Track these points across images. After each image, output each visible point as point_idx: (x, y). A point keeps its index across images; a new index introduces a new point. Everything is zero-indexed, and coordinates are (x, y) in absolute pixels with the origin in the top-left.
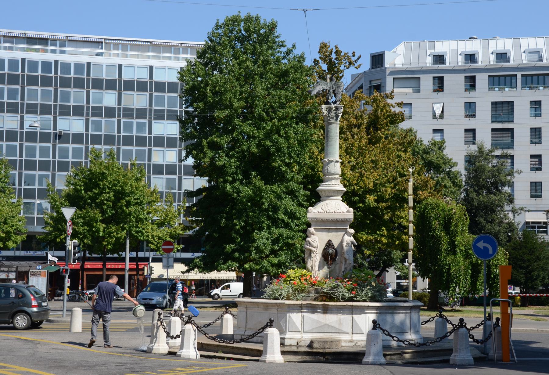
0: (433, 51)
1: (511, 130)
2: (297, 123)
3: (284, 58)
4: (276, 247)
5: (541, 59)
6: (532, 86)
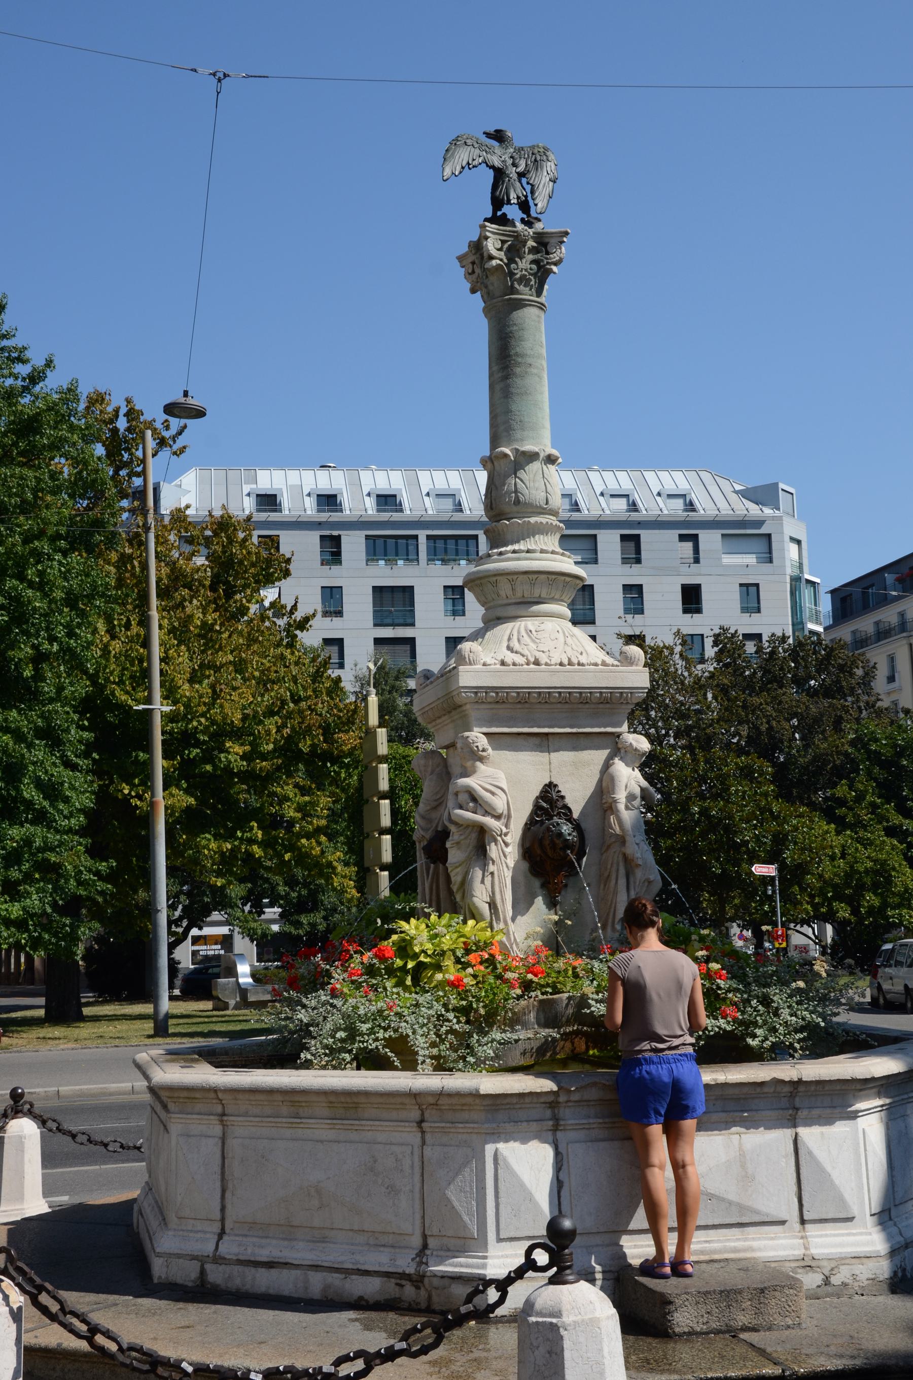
0: (254, 486)
1: (411, 642)
3: (25, 389)
4: (15, 874)
5: (459, 508)
6: (446, 558)
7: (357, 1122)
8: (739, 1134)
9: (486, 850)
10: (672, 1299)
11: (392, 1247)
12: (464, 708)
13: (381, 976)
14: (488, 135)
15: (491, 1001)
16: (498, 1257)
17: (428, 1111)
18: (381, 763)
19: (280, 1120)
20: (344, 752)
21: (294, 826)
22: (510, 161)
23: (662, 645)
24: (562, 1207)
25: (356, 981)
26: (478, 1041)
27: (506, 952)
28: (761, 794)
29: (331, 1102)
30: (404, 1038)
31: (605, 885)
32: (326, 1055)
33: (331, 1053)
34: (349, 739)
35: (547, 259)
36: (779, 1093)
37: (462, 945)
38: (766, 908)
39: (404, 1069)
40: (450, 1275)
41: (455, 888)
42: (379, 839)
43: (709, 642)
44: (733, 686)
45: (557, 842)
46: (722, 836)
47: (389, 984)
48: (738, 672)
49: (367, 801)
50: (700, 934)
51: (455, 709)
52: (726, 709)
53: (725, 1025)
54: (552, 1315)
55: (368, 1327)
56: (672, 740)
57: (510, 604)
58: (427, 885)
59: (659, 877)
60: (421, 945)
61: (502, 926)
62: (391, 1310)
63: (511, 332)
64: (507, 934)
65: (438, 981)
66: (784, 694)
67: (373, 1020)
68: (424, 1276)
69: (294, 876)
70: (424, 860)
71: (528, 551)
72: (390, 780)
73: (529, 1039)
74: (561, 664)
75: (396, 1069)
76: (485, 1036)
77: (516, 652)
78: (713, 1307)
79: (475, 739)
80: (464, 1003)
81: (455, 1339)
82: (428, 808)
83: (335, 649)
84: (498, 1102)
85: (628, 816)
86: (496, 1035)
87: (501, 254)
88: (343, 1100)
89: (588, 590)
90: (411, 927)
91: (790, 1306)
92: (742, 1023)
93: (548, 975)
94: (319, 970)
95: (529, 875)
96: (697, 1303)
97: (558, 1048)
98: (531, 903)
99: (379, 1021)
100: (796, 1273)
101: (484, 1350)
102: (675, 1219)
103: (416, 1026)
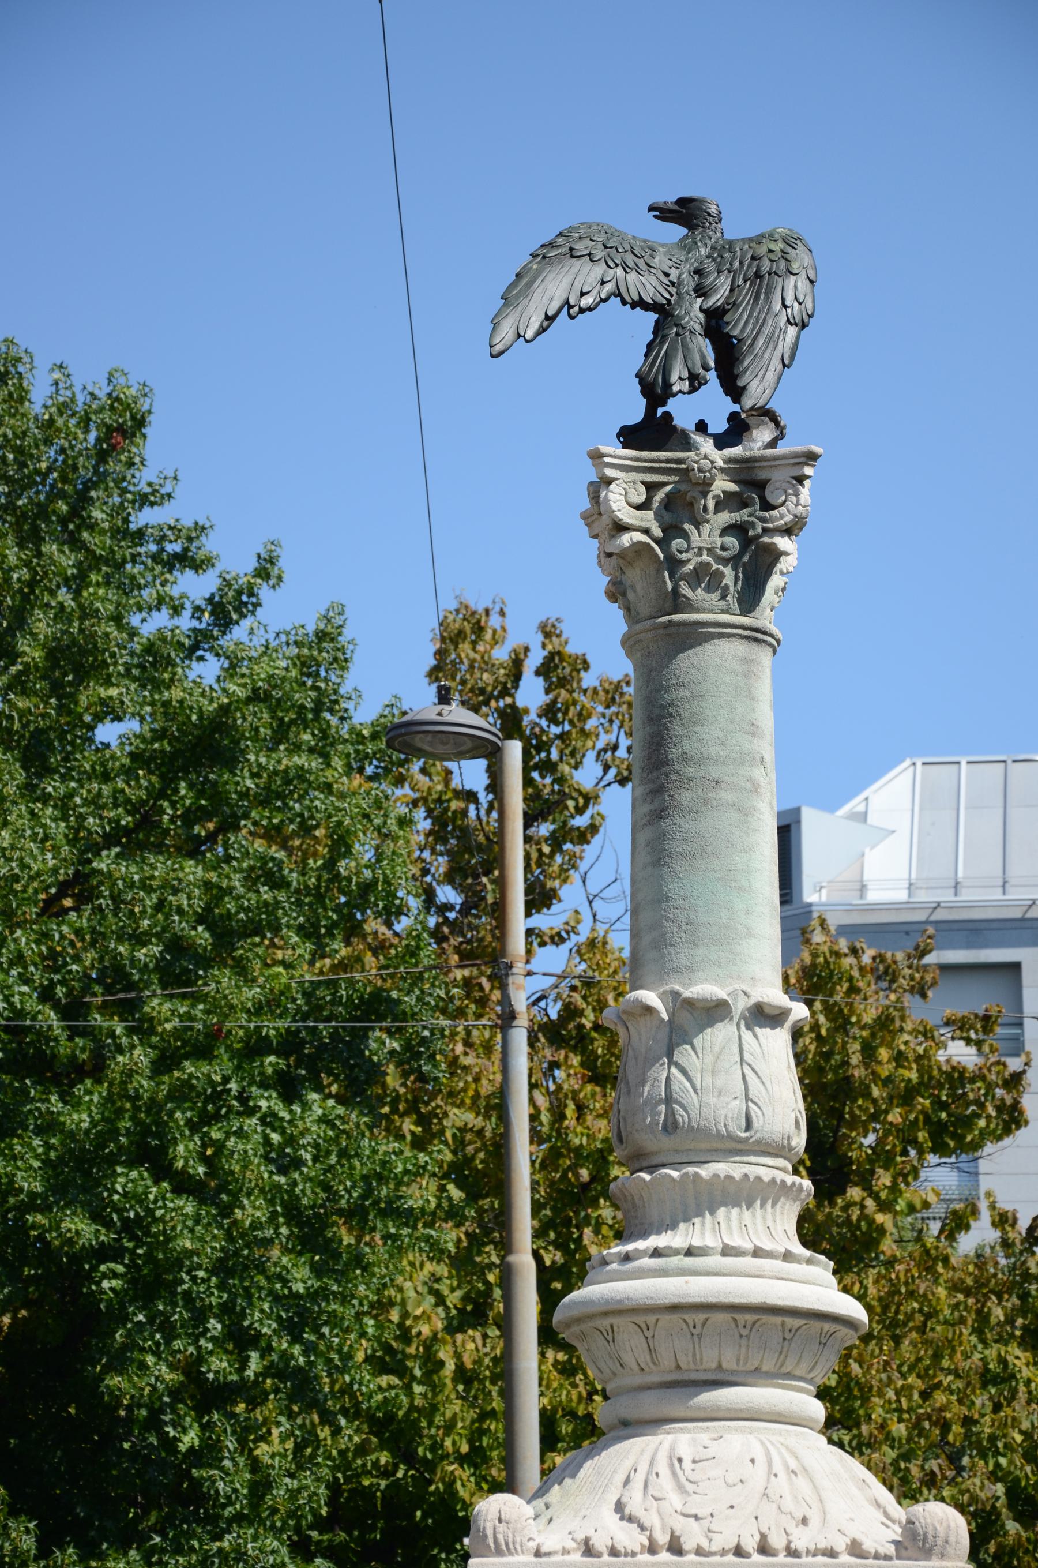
2: (289, 1089)
3: (198, 644)
14: (663, 213)
22: (689, 283)
35: (763, 520)
57: (649, 1387)
63: (672, 704)
71: (689, 1252)
74: (739, 1552)
77: (630, 1519)
87: (648, 519)
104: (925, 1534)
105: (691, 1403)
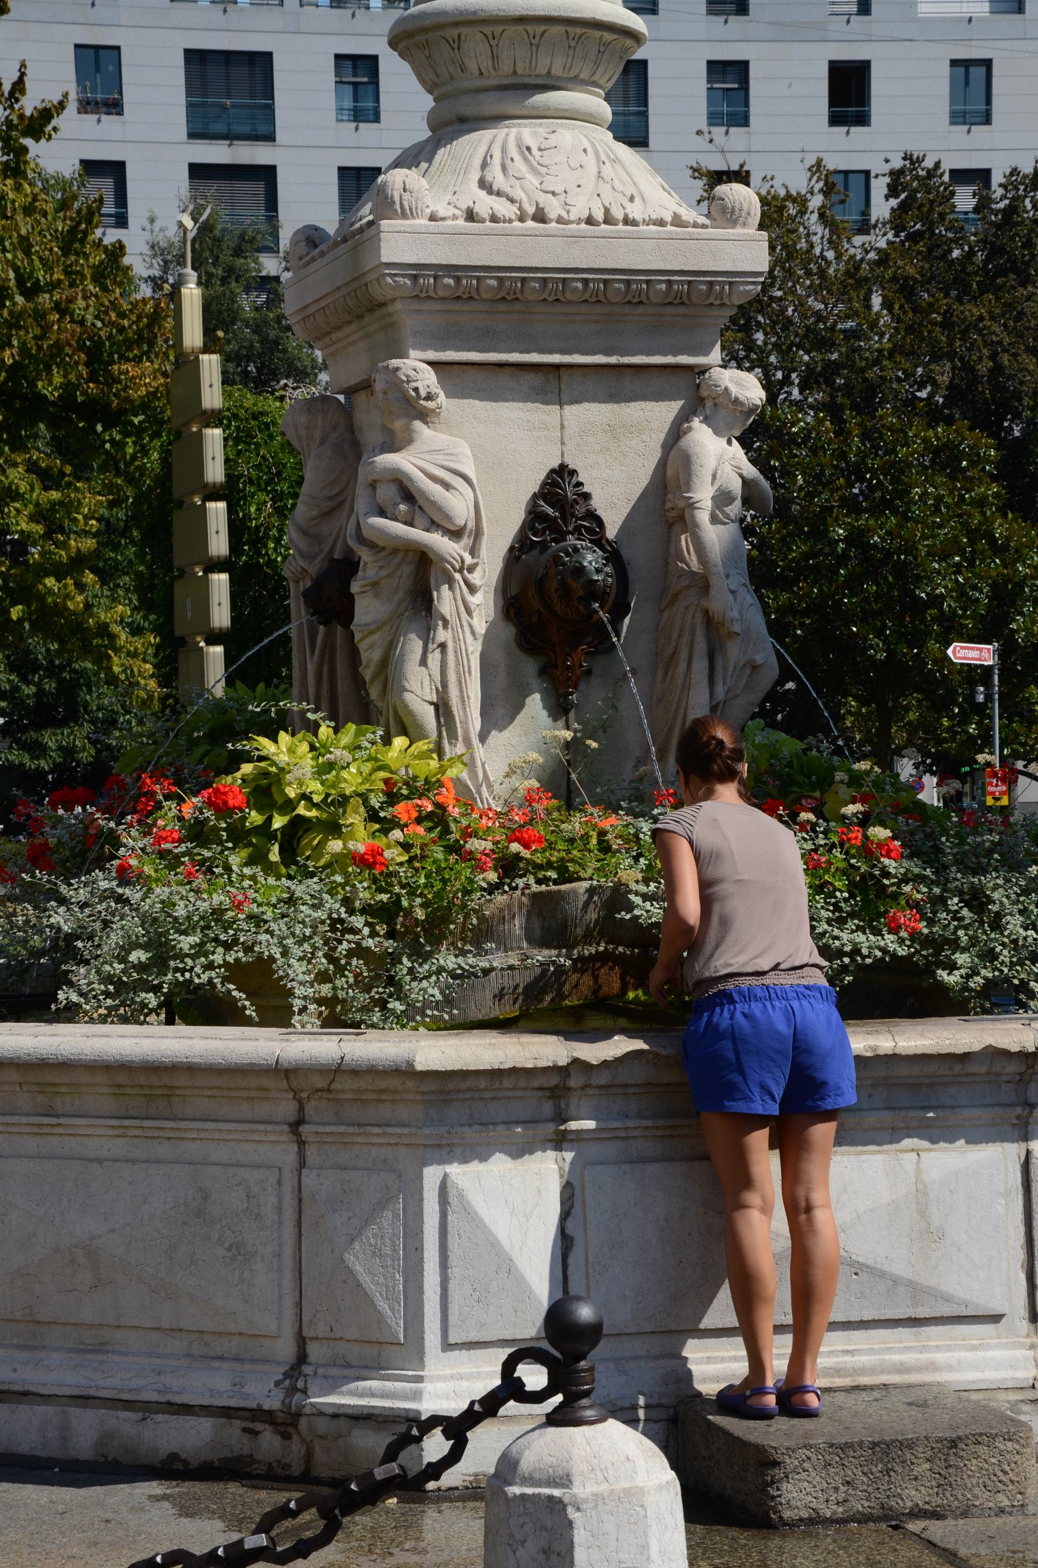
1: (267, 174)
7: (171, 1124)
8: (918, 1152)
9: (431, 600)
10: (779, 1458)
11: (237, 1359)
12: (390, 309)
13: (220, 843)
15: (438, 895)
16: (445, 1379)
17: (313, 1103)
18: (207, 426)
19: (16, 1119)
20: (132, 402)
21: (26, 552)
23: (782, 193)
24: (571, 1284)
25: (170, 851)
26: (411, 971)
27: (467, 800)
28: (973, 502)
29: (119, 1086)
30: (265, 964)
31: (666, 674)
32: (107, 994)
33: (118, 993)
34: (142, 377)
36: (997, 1075)
37: (382, 786)
38: (972, 729)
39: (264, 1022)
40: (349, 1411)
41: (367, 674)
42: (205, 580)
43: (879, 187)
44: (926, 281)
45: (573, 584)
46: (891, 587)
47: (235, 860)
48: (937, 250)
49: (180, 504)
50: (850, 771)
51: (371, 310)
52: (909, 330)
53: (896, 946)
54: (551, 1482)
55: (187, 1511)
56: (796, 392)
57: (486, 90)
58: (311, 667)
59: (773, 659)
60: (301, 784)
61: (460, 749)
62: (233, 1479)
64: (471, 765)
65: (333, 855)
66: (1029, 298)
67: (203, 929)
68: (299, 1415)
69: (28, 652)
70: (305, 618)
72: (227, 461)
73: (511, 968)
74: (590, 221)
75: (248, 1022)
76: (425, 961)
77: (499, 194)
78: (858, 1472)
79: (412, 373)
80: (384, 897)
81: (357, 1530)
82: (315, 513)
83: (106, 186)
84: (451, 1086)
85: (716, 536)
86: (448, 960)
88: (142, 1081)
89: (636, 74)
90: (282, 749)
91: (1005, 1473)
92: (927, 941)
93: (551, 846)
94: (92, 831)
95: (516, 650)
96: (828, 1465)
97: (567, 987)
98: (517, 707)
99: (216, 930)
100: (1020, 1413)
101: (414, 1550)
102: (789, 1309)
103: (289, 941)
104: (733, 208)
105: (530, 100)
